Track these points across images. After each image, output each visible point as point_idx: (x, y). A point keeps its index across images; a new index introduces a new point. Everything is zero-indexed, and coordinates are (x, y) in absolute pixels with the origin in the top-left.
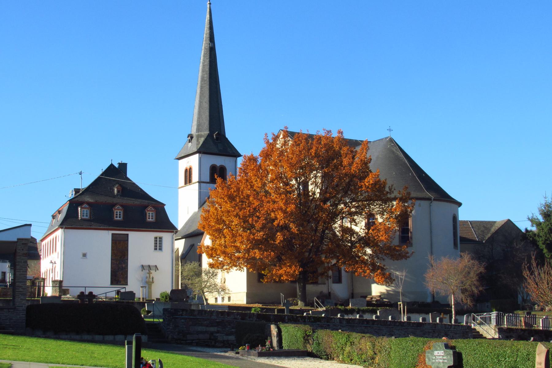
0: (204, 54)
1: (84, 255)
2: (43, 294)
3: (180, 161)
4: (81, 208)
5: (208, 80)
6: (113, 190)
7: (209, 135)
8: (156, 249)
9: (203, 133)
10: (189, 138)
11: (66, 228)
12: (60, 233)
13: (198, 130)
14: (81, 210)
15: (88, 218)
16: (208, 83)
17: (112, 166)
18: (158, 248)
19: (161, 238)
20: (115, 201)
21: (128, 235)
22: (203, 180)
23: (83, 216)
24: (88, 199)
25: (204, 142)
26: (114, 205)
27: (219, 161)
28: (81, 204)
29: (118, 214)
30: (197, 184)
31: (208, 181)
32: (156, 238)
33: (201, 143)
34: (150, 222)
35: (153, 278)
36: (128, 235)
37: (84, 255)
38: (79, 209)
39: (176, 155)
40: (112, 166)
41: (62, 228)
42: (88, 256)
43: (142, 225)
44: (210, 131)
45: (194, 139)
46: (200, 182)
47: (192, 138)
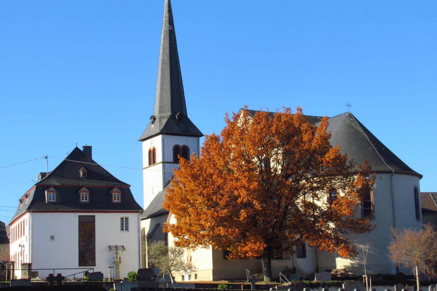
0: (164, 37)
1: (52, 238)
2: (13, 278)
3: (144, 143)
4: (48, 192)
5: (168, 62)
6: (79, 173)
7: (171, 116)
8: (122, 229)
9: (165, 115)
10: (152, 120)
11: (33, 212)
12: (27, 216)
13: (160, 111)
14: (47, 193)
15: (55, 201)
16: (169, 65)
17: (77, 149)
18: (124, 228)
19: (127, 219)
20: (81, 183)
21: (94, 216)
22: (166, 160)
23: (50, 199)
24: (54, 182)
25: (167, 123)
26: (80, 188)
27: (182, 141)
28: (47, 187)
29: (84, 197)
30: (161, 164)
31: (172, 161)
32: (122, 219)
33: (164, 124)
34: (116, 204)
35: (120, 258)
36: (94, 216)
37: (52, 238)
38: (46, 192)
39: (139, 137)
40: (77, 149)
41: (29, 212)
42: (56, 238)
43: (109, 207)
44: (172, 112)
45: (157, 121)
46: (163, 162)
47: (154, 119)
